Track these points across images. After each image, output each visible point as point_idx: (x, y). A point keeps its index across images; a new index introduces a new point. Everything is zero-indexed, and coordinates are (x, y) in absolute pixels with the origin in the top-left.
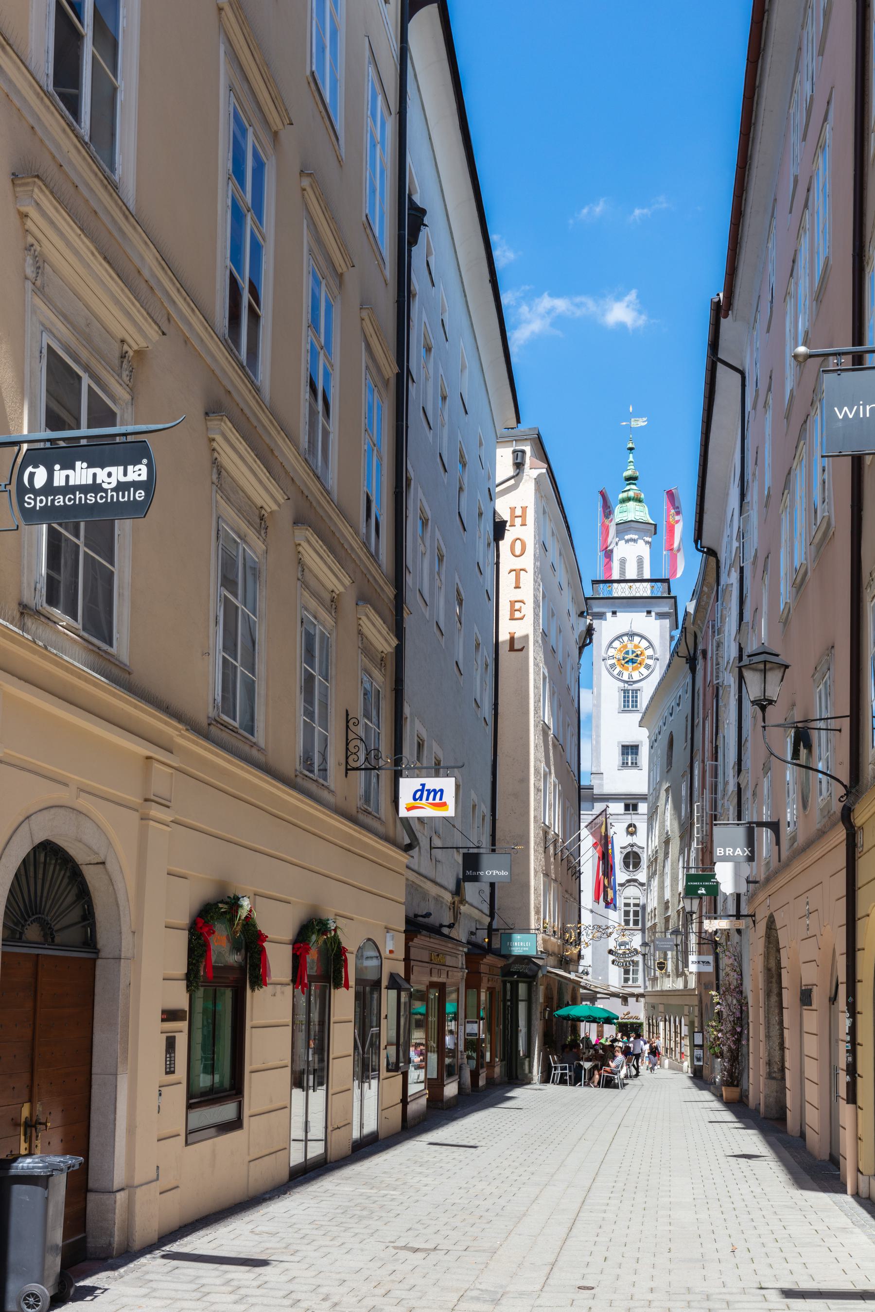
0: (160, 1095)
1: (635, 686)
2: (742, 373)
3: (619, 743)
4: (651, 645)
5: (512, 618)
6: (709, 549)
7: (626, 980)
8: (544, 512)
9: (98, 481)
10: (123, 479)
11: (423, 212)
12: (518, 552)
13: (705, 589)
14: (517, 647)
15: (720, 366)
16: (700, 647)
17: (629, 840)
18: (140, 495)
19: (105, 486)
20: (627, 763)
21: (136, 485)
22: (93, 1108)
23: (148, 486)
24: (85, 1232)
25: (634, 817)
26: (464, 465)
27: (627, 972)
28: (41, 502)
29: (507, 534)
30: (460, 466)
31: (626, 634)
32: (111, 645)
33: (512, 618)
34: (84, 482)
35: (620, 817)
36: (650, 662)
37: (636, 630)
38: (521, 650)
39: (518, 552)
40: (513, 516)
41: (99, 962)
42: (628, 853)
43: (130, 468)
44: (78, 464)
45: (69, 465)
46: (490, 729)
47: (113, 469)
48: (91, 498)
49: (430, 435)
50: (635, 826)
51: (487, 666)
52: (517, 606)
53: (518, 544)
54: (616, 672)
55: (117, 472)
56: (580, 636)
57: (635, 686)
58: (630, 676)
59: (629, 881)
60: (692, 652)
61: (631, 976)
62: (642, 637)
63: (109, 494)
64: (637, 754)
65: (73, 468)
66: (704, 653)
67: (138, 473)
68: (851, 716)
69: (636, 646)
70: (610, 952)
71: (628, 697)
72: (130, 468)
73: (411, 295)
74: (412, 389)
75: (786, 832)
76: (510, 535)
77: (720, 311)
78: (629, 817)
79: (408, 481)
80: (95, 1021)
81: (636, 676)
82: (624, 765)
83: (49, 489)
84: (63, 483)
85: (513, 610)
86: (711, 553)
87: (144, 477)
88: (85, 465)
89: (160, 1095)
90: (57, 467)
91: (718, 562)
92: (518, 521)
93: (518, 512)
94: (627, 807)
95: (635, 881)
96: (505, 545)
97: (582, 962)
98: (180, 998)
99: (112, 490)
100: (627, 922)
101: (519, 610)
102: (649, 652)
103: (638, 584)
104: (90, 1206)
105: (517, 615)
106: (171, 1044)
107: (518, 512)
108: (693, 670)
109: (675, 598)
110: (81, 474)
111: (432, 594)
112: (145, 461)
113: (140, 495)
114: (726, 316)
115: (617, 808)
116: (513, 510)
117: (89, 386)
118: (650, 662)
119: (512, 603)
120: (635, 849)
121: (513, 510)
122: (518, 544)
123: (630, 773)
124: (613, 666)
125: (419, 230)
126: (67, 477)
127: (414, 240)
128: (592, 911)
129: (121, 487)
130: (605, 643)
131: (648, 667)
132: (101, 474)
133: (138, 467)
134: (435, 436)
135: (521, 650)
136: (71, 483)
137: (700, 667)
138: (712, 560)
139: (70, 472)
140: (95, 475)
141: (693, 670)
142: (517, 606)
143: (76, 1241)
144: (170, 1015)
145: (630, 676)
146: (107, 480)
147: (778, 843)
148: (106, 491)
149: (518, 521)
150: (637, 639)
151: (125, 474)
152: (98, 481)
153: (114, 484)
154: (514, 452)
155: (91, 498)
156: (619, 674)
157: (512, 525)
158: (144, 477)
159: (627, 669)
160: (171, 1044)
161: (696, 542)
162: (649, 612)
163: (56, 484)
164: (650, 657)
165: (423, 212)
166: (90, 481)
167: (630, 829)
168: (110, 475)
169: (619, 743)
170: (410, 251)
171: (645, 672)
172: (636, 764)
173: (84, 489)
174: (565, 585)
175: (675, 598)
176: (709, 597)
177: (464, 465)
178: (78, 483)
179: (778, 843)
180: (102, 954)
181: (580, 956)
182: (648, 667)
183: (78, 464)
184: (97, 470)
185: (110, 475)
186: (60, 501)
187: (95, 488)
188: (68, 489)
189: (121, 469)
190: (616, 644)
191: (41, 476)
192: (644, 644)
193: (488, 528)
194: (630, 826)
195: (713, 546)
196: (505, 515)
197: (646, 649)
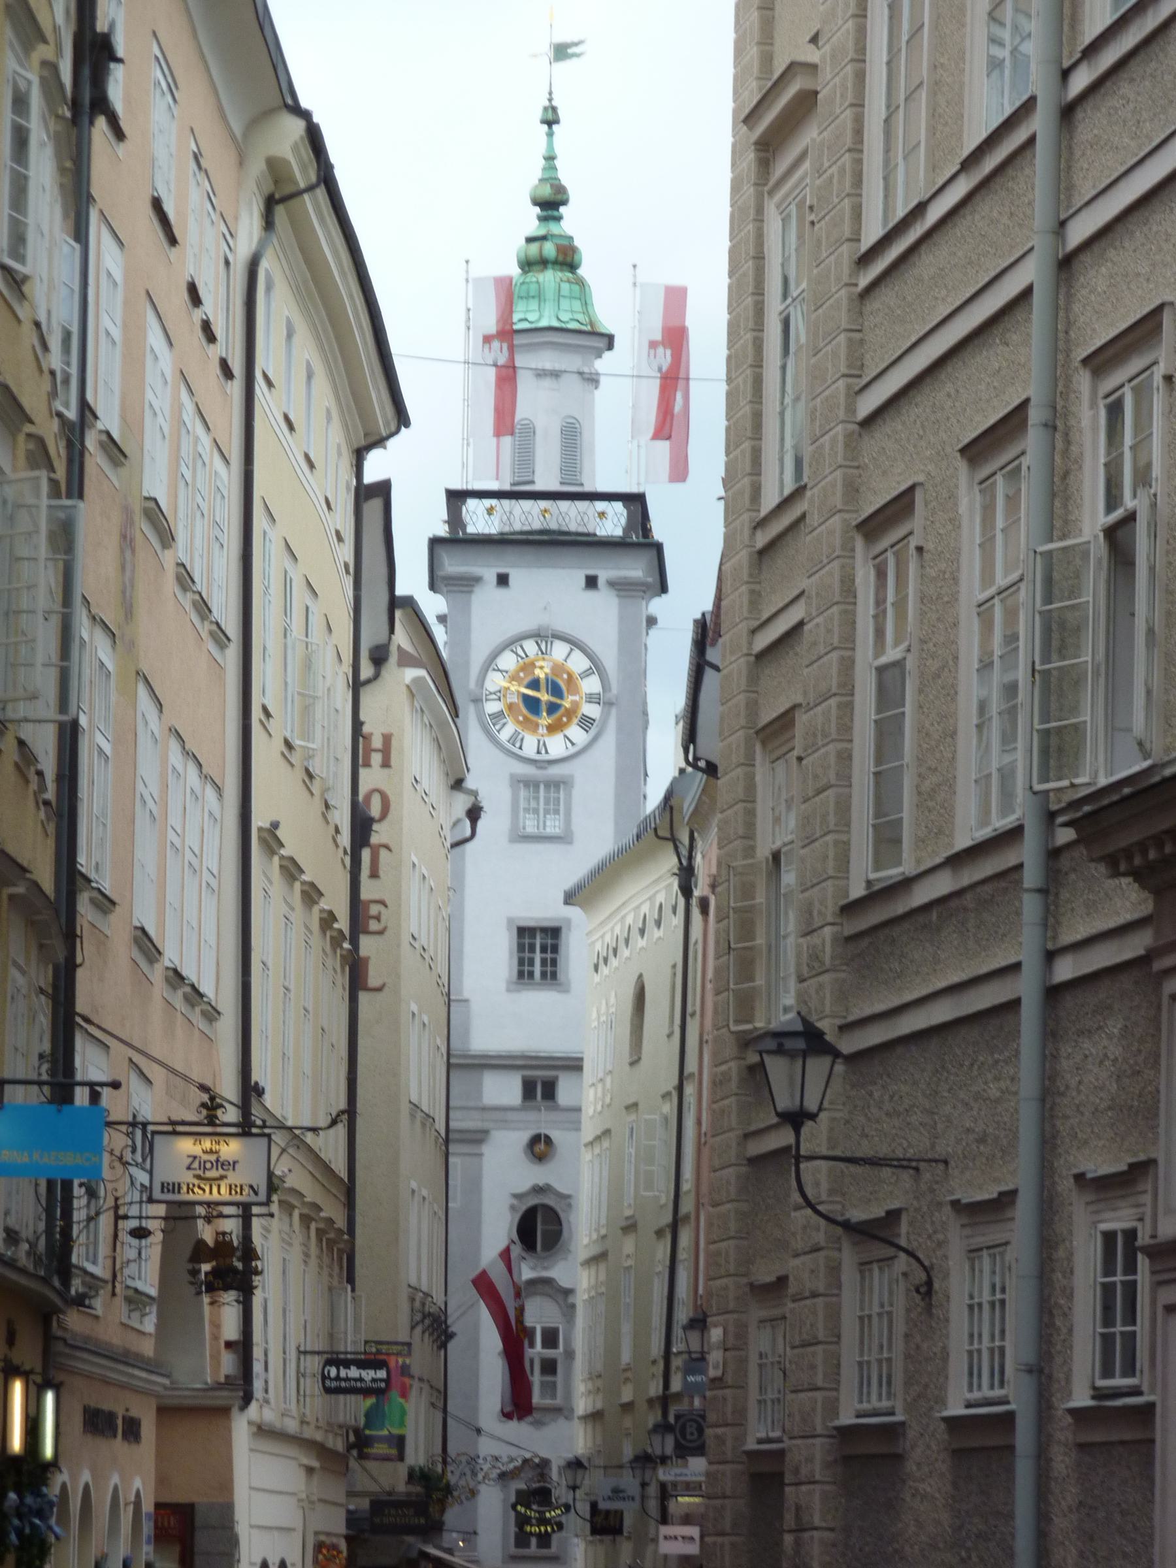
0: (551, 120)
1: (555, 771)
3: (510, 921)
4: (597, 666)
6: (708, 763)
17: (527, 1176)
18: (383, 1385)
20: (531, 974)
21: (381, 1380)
23: (387, 1381)
25: (544, 1115)
28: (334, 1384)
35: (510, 1116)
38: (379, 989)
45: (347, 1367)
50: (548, 1140)
54: (504, 736)
58: (541, 748)
62: (575, 644)
64: (555, 949)
67: (382, 1374)
69: (558, 668)
71: (537, 799)
78: (531, 1116)
83: (338, 1378)
89: (551, 120)
95: (548, 1281)
102: (592, 685)
110: (354, 1372)
115: (504, 1090)
120: (549, 1201)
123: (539, 999)
124: (499, 715)
128: (479, 1431)
129: (374, 1380)
130: (477, 658)
131: (586, 723)
135: (379, 989)
145: (541, 748)
150: (559, 650)
155: (359, 1384)
156: (513, 740)
159: (534, 728)
162: (591, 582)
164: (592, 699)
167: (537, 1149)
169: (510, 921)
171: (575, 732)
172: (554, 975)
173: (356, 1380)
175: (658, 548)
182: (586, 723)
186: (343, 1384)
187: (361, 1379)
188: (347, 1379)
190: (508, 661)
191: (333, 1372)
192: (578, 663)
194: (535, 1140)
197: (587, 674)
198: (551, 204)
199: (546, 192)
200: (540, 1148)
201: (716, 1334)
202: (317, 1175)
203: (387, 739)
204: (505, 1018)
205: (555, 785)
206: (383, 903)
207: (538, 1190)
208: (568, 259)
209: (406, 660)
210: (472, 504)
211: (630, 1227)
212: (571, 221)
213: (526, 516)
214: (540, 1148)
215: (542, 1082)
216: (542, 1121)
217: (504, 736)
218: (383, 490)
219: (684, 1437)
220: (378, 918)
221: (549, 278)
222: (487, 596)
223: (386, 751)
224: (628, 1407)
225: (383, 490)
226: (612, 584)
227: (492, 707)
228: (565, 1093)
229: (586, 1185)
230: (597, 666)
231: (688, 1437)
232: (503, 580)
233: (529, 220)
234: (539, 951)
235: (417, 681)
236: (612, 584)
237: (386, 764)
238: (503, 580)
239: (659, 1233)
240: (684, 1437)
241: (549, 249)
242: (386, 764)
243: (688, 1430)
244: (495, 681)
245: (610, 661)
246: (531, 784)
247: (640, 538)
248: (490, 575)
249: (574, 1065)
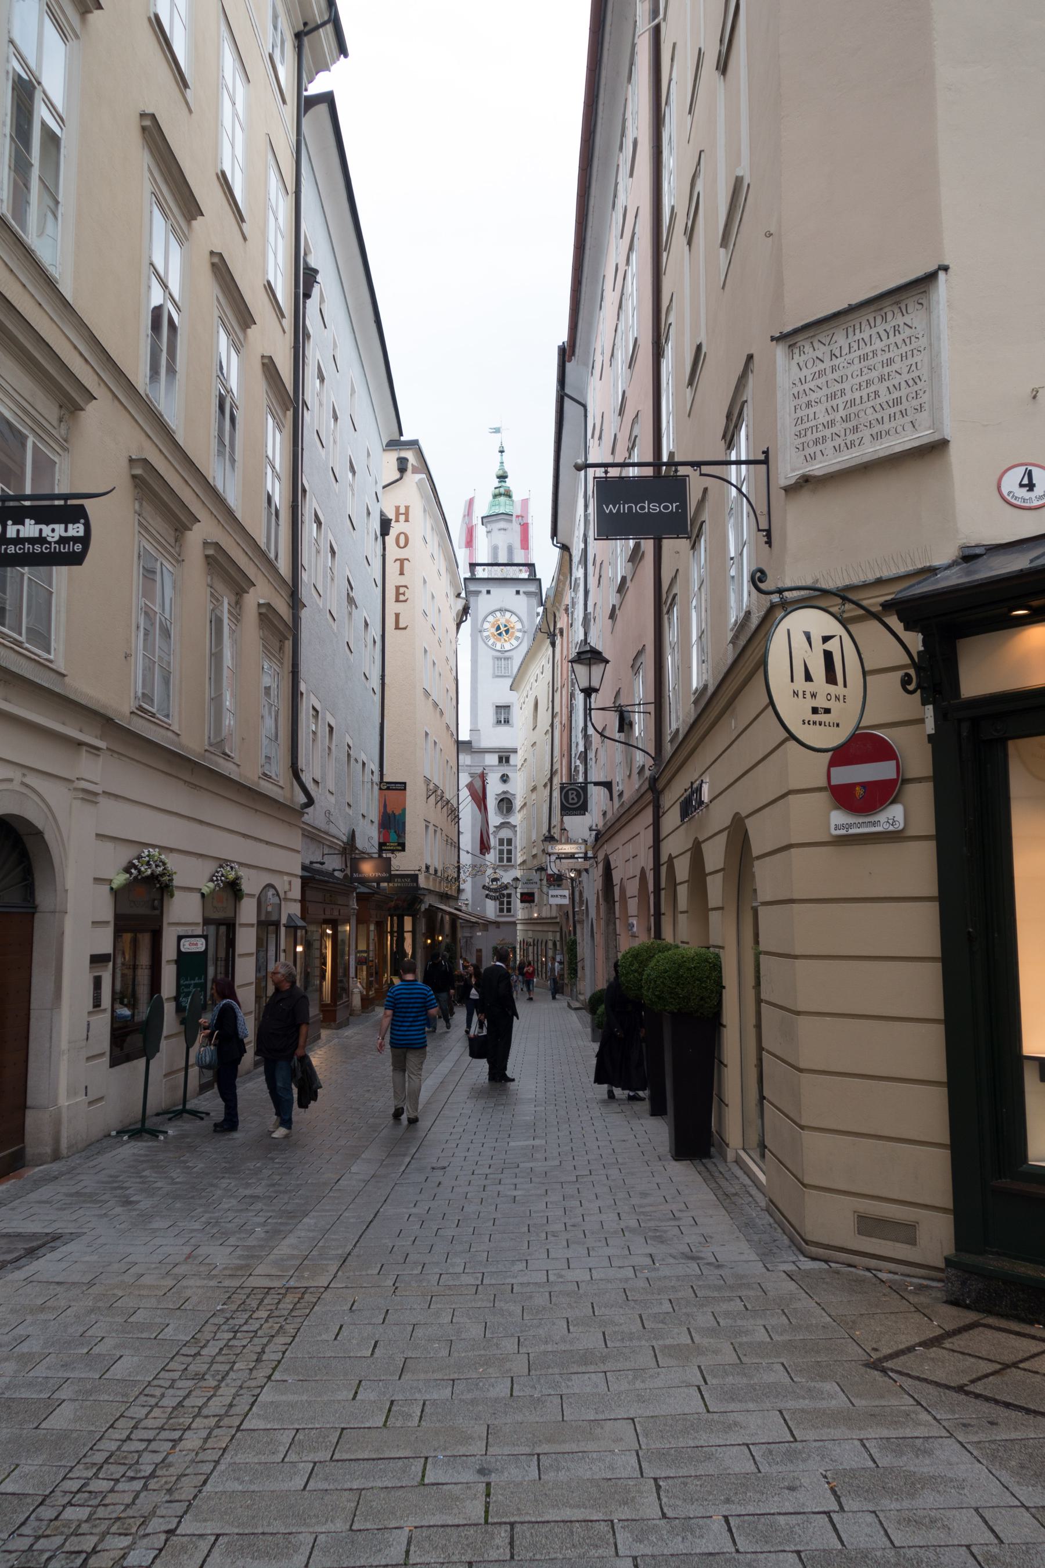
1: (507, 654)
2: (584, 406)
4: (520, 620)
5: (397, 600)
7: (501, 910)
8: (425, 511)
9: (44, 535)
10: (64, 534)
11: (316, 271)
12: (402, 544)
13: (561, 577)
14: (401, 626)
15: (566, 399)
16: (558, 626)
18: (78, 548)
19: (49, 539)
21: (75, 539)
22: (31, 1038)
24: (23, 1142)
26: (354, 472)
27: (501, 903)
29: (392, 531)
30: (350, 475)
31: (500, 610)
32: (49, 653)
33: (397, 600)
34: (32, 535)
36: (519, 634)
37: (508, 608)
38: (405, 628)
39: (402, 544)
40: (398, 514)
41: (37, 916)
42: (502, 800)
43: (70, 526)
44: (27, 521)
46: (377, 698)
47: (56, 526)
48: (38, 548)
49: (322, 452)
51: (375, 642)
52: (402, 590)
53: (402, 537)
54: (490, 643)
55: (59, 528)
56: (457, 615)
57: (507, 654)
58: (502, 646)
59: (502, 823)
60: (552, 629)
61: (505, 906)
63: (53, 546)
65: (23, 525)
66: (561, 631)
67: (76, 530)
68: (655, 703)
70: (484, 887)
72: (70, 526)
73: (307, 336)
74: (307, 415)
75: (616, 789)
76: (395, 529)
77: (566, 354)
78: (502, 768)
79: (304, 491)
80: (33, 965)
81: (507, 647)
82: (499, 722)
84: (14, 535)
85: (398, 594)
86: (565, 548)
87: (81, 533)
88: (33, 522)
90: (10, 522)
91: (571, 556)
92: (402, 518)
93: (402, 510)
94: (500, 759)
96: (390, 539)
97: (463, 896)
98: (104, 942)
99: (55, 542)
100: (501, 860)
101: (404, 594)
103: (508, 568)
104: (29, 1121)
105: (402, 598)
106: (97, 982)
107: (402, 510)
108: (553, 644)
109: (539, 580)
110: (30, 529)
111: (325, 587)
112: (82, 521)
113: (78, 548)
114: (570, 361)
115: (492, 759)
116: (397, 508)
117: (34, 443)
118: (519, 634)
119: (398, 588)
120: (508, 796)
121: (397, 508)
122: (402, 537)
123: (503, 729)
124: (487, 637)
125: (313, 286)
126: (18, 531)
127: (307, 295)
129: (63, 540)
131: (517, 638)
132: (46, 530)
133: (77, 525)
134: (327, 454)
135: (405, 628)
136: (21, 535)
137: (558, 642)
138: (566, 554)
139: (20, 527)
140: (41, 531)
141: (553, 644)
142: (402, 590)
143: (13, 1153)
144: (97, 960)
146: (51, 534)
147: (611, 799)
148: (50, 543)
149: (402, 518)
150: (508, 615)
151: (66, 530)
152: (44, 535)
153: (57, 538)
154: (398, 459)
155: (38, 548)
157: (397, 521)
158: (81, 533)
160: (97, 982)
161: (553, 539)
162: (518, 592)
163: (9, 535)
164: (519, 631)
165: (316, 271)
166: (37, 535)
168: (53, 530)
170: (304, 303)
171: (515, 643)
172: (507, 722)
173: (32, 541)
174: (443, 571)
175: (539, 580)
176: (564, 584)
177: (354, 472)
178: (27, 536)
179: (611, 799)
180: (40, 909)
181: (459, 891)
182: (517, 638)
183: (27, 521)
184: (43, 527)
185: (53, 530)
187: (41, 540)
188: (18, 541)
189: (63, 526)
190: (490, 619)
192: (514, 619)
193: (376, 526)
194: (503, 776)
195: (567, 544)
196: (391, 515)
198: (502, 477)
199: (501, 473)
200: (505, 779)
201: (437, 1425)
202: (82, 348)
203: (407, 508)
204: (494, 737)
205: (507, 659)
206: (406, 587)
207: (504, 793)
208: (508, 494)
209: (415, 471)
210: (478, 568)
211: (534, 789)
212: (509, 483)
213: (497, 572)
214: (505, 779)
215: (504, 757)
216: (504, 769)
217: (490, 643)
218: (328, 99)
219: (567, 801)
220: (404, 594)
221: (502, 499)
222: (483, 596)
223: (407, 514)
224: (534, 856)
225: (328, 99)
226: (525, 593)
227: (485, 634)
228: (512, 761)
229: (518, 787)
230: (520, 620)
231: (571, 801)
232: (488, 592)
233: (496, 482)
234: (503, 714)
235: (420, 480)
236: (525, 593)
237: (407, 520)
238: (488, 592)
239: (545, 786)
240: (567, 801)
241: (502, 490)
242: (407, 520)
243: (571, 797)
244: (486, 625)
245: (524, 618)
246: (499, 659)
247: (534, 579)
248: (484, 591)
249: (515, 751)
